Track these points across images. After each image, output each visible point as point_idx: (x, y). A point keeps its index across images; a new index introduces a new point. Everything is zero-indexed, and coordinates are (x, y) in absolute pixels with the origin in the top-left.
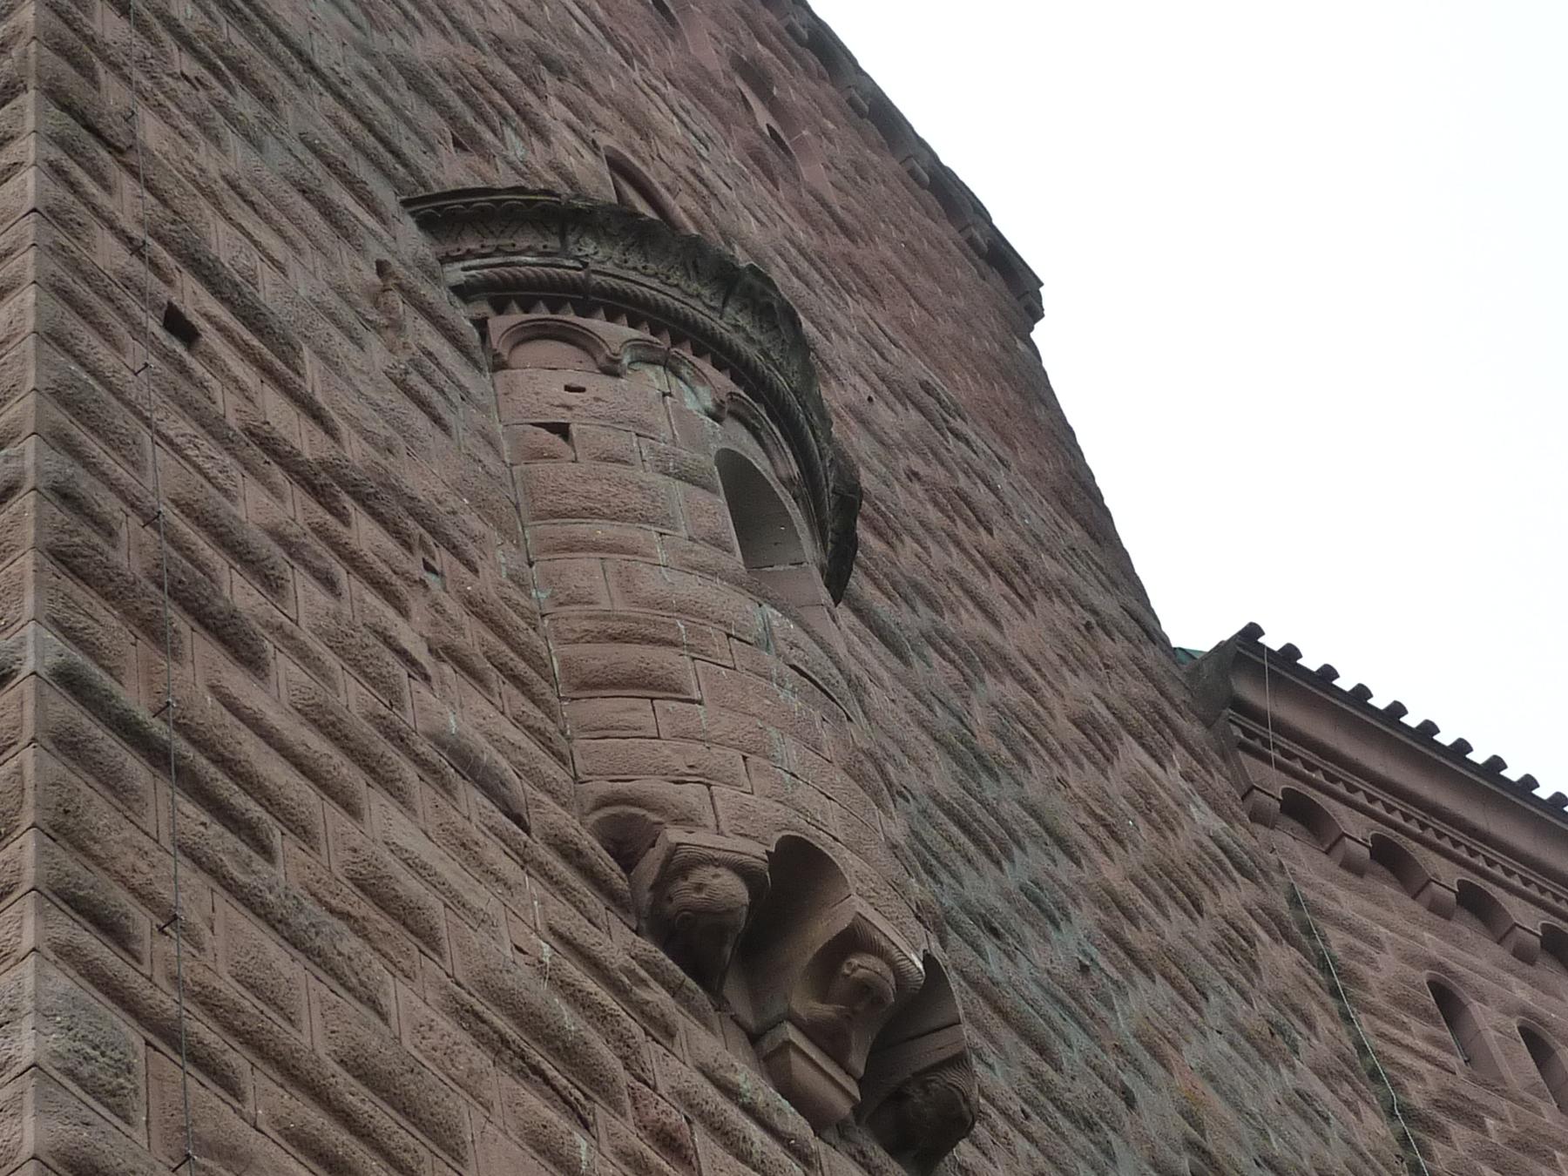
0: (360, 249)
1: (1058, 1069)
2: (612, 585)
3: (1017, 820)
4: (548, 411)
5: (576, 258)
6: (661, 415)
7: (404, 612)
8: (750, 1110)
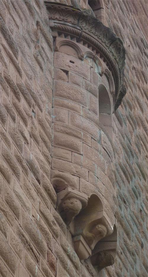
0: (34, 18)
1: (130, 239)
2: (70, 118)
3: (135, 169)
4: (65, 66)
5: (80, 27)
6: (89, 71)
7: (26, 125)
8: (69, 256)
